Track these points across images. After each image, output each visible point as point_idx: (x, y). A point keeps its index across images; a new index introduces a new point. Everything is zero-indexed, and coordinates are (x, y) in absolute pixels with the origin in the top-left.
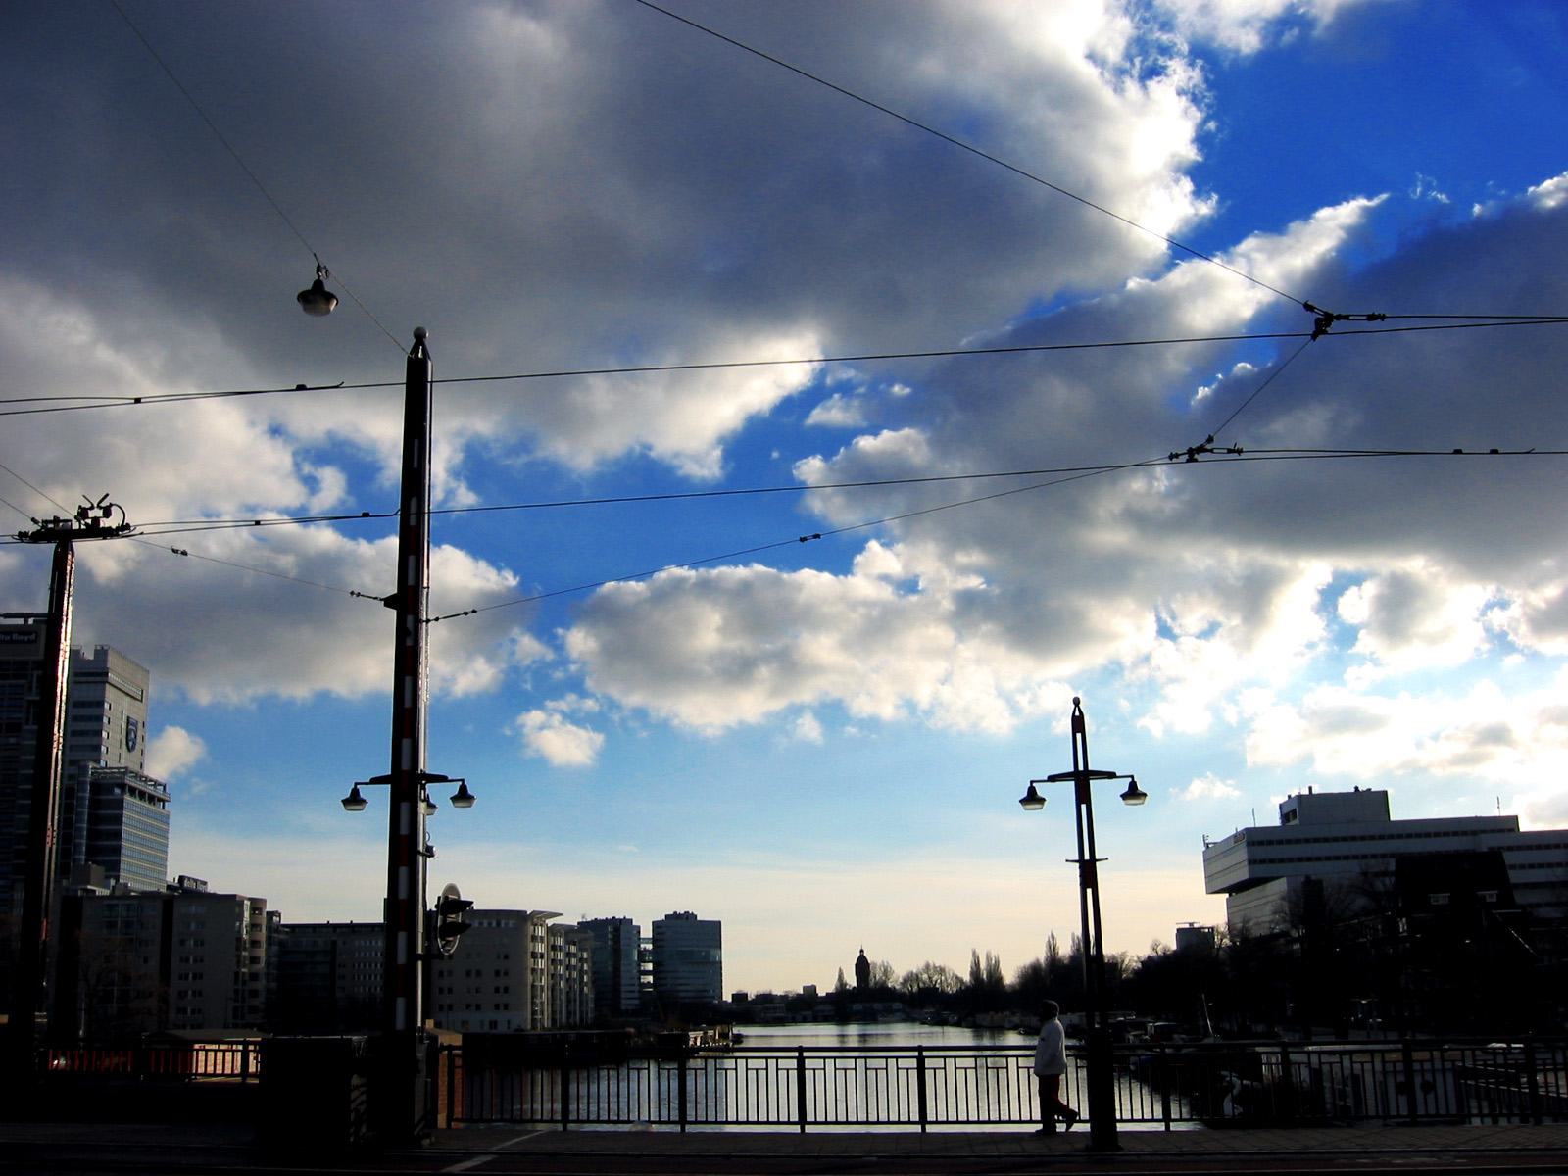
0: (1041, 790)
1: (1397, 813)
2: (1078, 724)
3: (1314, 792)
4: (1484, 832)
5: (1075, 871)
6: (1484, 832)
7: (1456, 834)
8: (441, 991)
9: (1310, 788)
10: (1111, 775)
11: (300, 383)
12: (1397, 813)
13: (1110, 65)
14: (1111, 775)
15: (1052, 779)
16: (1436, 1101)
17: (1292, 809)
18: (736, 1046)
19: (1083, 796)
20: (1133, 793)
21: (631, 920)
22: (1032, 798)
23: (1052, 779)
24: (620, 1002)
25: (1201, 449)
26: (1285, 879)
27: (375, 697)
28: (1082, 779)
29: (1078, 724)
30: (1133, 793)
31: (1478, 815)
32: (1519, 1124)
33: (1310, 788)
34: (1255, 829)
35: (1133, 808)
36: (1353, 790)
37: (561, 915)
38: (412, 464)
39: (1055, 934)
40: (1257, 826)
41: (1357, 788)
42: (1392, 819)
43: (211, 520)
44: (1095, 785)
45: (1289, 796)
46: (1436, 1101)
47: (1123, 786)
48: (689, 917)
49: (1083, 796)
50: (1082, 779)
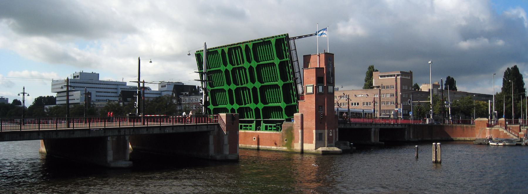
0: (20, 94)
1: (101, 79)
2: (24, 88)
3: (83, 72)
4: (119, 85)
6: (119, 85)
7: (114, 85)
8: (352, 104)
9: (83, 71)
10: (26, 93)
12: (101, 79)
13: (48, 109)
14: (26, 93)
15: (21, 93)
18: (211, 80)
19: (24, 95)
20: (28, 95)
21: (126, 83)
22: (19, 95)
23: (21, 93)
25: (245, 137)
26: (80, 91)
28: (24, 93)
29: (24, 88)
30: (28, 95)
33: (83, 71)
35: (28, 96)
37: (205, 43)
38: (137, 93)
42: (100, 79)
44: (25, 94)
47: (27, 94)
48: (15, 100)
49: (24, 95)
50: (24, 93)
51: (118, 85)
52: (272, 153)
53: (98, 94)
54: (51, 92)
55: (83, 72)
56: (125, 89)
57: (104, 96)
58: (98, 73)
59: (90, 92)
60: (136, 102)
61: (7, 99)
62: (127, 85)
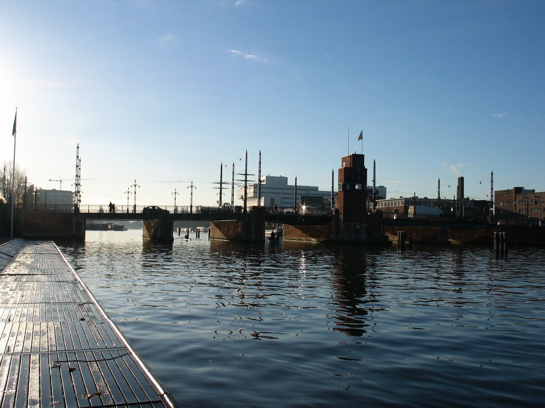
1: (536, 192)
3: (270, 176)
5: (191, 193)
6: (310, 190)
9: (269, 175)
11: (401, 196)
12: (536, 192)
16: (288, 198)
17: (263, 179)
24: (238, 208)
27: (248, 201)
29: (492, 174)
30: (224, 195)
31: (308, 186)
32: (494, 190)
33: (269, 175)
34: (314, 187)
36: (279, 176)
39: (416, 193)
40: (315, 186)
41: (280, 176)
42: (288, 185)
43: (52, 211)
45: (280, 176)
46: (288, 198)
47: (29, 183)
51: (308, 190)
52: (507, 309)
53: (285, 200)
54: (34, 185)
55: (270, 176)
56: (316, 195)
57: (288, 203)
58: (532, 189)
59: (273, 198)
60: (492, 209)
61: (286, 179)
62: (319, 190)
